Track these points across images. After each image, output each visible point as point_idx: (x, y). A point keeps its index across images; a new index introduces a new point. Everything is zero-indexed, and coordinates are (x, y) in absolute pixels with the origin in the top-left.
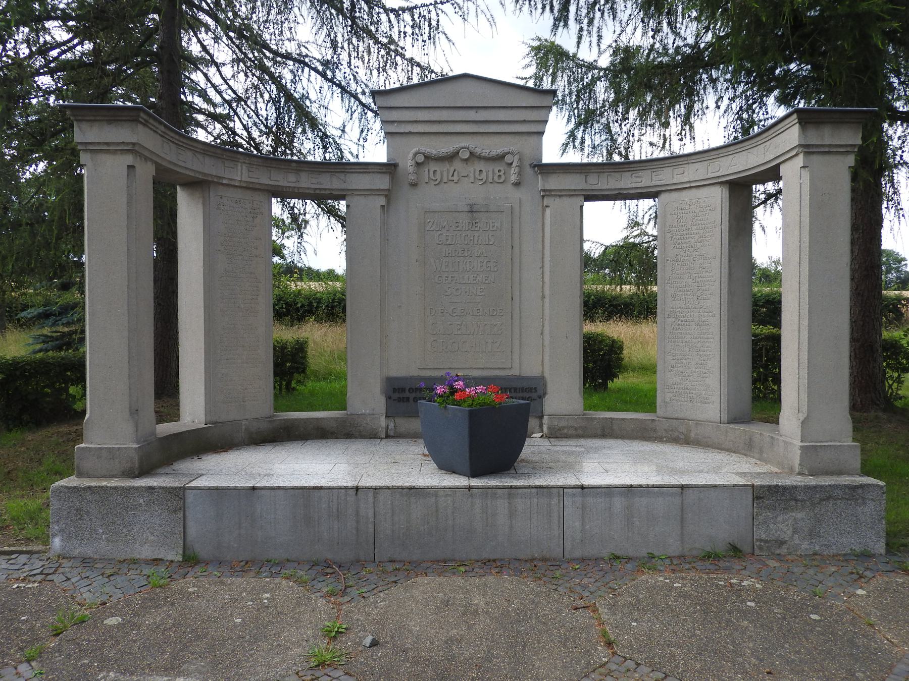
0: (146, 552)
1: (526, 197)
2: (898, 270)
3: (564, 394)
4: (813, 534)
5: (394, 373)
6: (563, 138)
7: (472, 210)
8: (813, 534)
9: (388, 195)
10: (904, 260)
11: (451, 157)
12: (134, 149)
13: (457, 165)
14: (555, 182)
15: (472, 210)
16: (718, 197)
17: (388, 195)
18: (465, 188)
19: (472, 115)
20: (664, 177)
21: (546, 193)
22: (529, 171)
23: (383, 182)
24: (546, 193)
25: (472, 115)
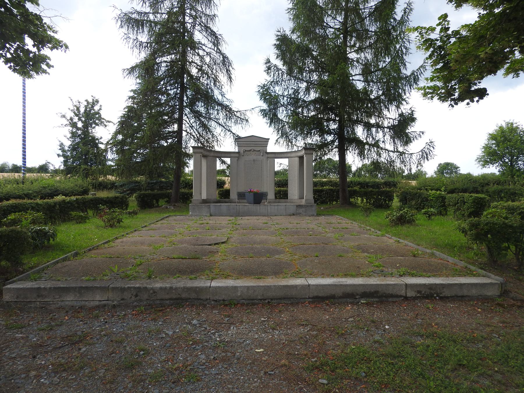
0: (204, 214)
1: (264, 158)
2: (456, 172)
3: (271, 196)
4: (305, 212)
5: (239, 191)
6: (275, 142)
7: (254, 161)
8: (305, 212)
9: (238, 158)
10: (459, 168)
11: (250, 150)
12: (201, 153)
13: (251, 152)
14: (269, 156)
15: (254, 161)
16: (297, 159)
17: (238, 158)
18: (253, 156)
19: (254, 143)
20: (289, 155)
21: (268, 158)
22: (265, 153)
23: (237, 155)
24: (268, 158)
25: (254, 143)
